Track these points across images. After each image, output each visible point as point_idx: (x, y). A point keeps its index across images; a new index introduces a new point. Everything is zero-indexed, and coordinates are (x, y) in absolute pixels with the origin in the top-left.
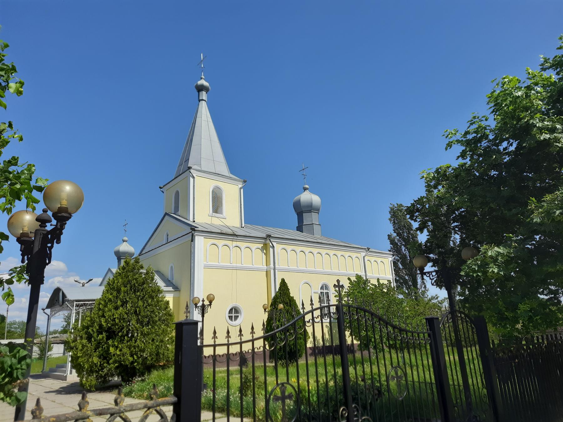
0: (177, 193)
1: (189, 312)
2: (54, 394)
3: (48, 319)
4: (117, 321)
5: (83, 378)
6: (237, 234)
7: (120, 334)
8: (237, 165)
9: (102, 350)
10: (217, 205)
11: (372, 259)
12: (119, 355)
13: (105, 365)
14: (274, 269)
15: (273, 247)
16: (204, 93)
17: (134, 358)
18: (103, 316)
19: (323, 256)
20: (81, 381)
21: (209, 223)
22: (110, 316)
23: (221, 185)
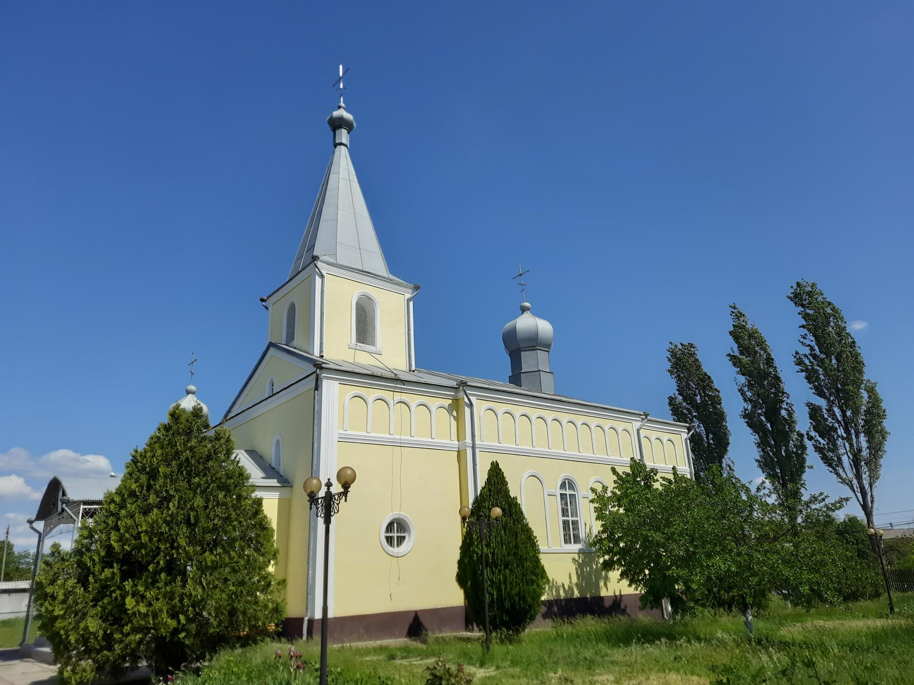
0: (292, 308)
3: (39, 541)
4: (144, 538)
7: (151, 568)
8: (404, 252)
9: (110, 603)
10: (365, 329)
11: (653, 435)
12: (146, 615)
14: (473, 448)
15: (471, 405)
16: (344, 132)
17: (179, 622)
18: (117, 528)
19: (564, 426)
23: (372, 292)
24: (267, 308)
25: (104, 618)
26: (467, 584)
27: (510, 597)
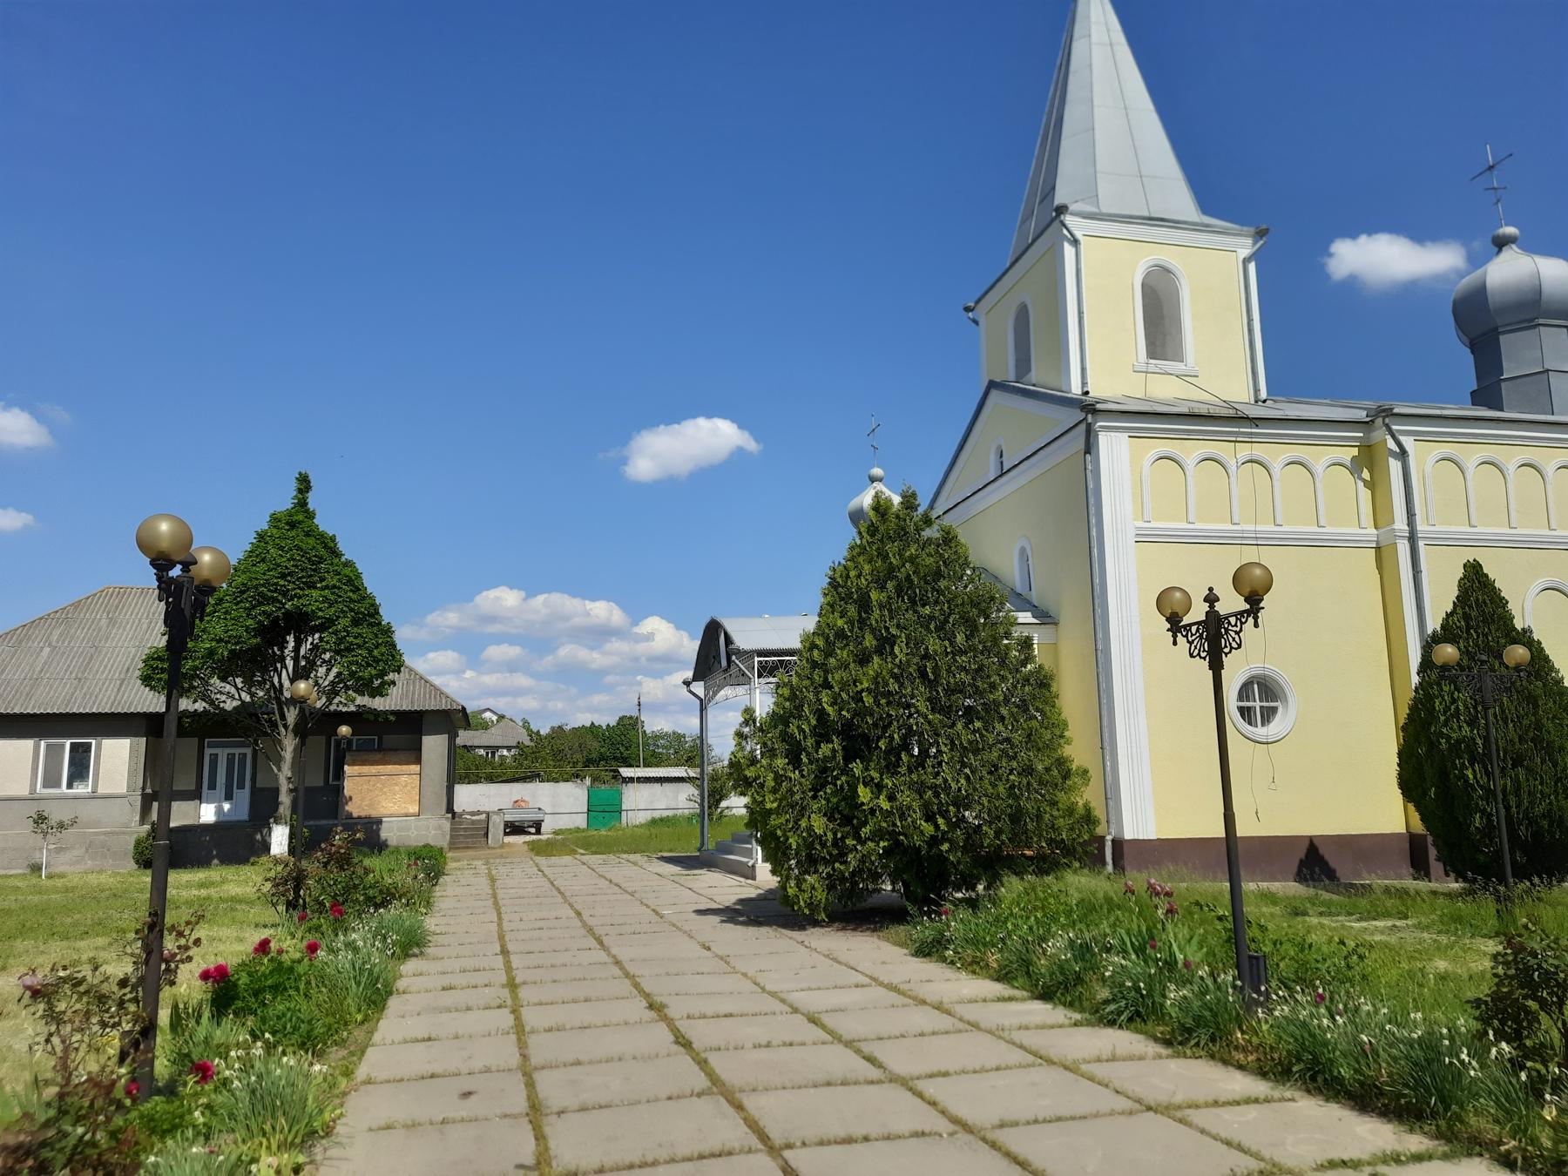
0: (1023, 315)
1: (544, 1137)
2: (717, 919)
4: (868, 700)
5: (788, 878)
7: (882, 744)
8: (1219, 189)
9: (834, 794)
12: (889, 813)
13: (850, 842)
14: (1412, 539)
15: (1403, 454)
17: (937, 827)
18: (827, 685)
20: (783, 887)
22: (844, 686)
24: (976, 322)
25: (830, 815)
26: (1425, 793)
27: (1532, 822)
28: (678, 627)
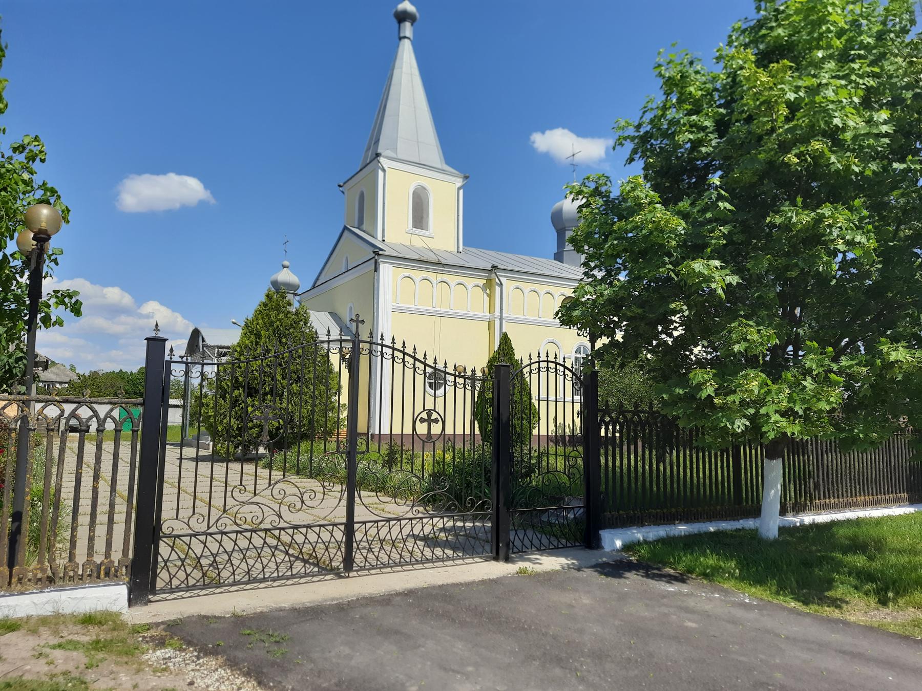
0: (362, 196)
6: (443, 262)
10: (420, 218)
14: (501, 319)
16: (408, 25)
21: (407, 244)
28: (173, 311)
